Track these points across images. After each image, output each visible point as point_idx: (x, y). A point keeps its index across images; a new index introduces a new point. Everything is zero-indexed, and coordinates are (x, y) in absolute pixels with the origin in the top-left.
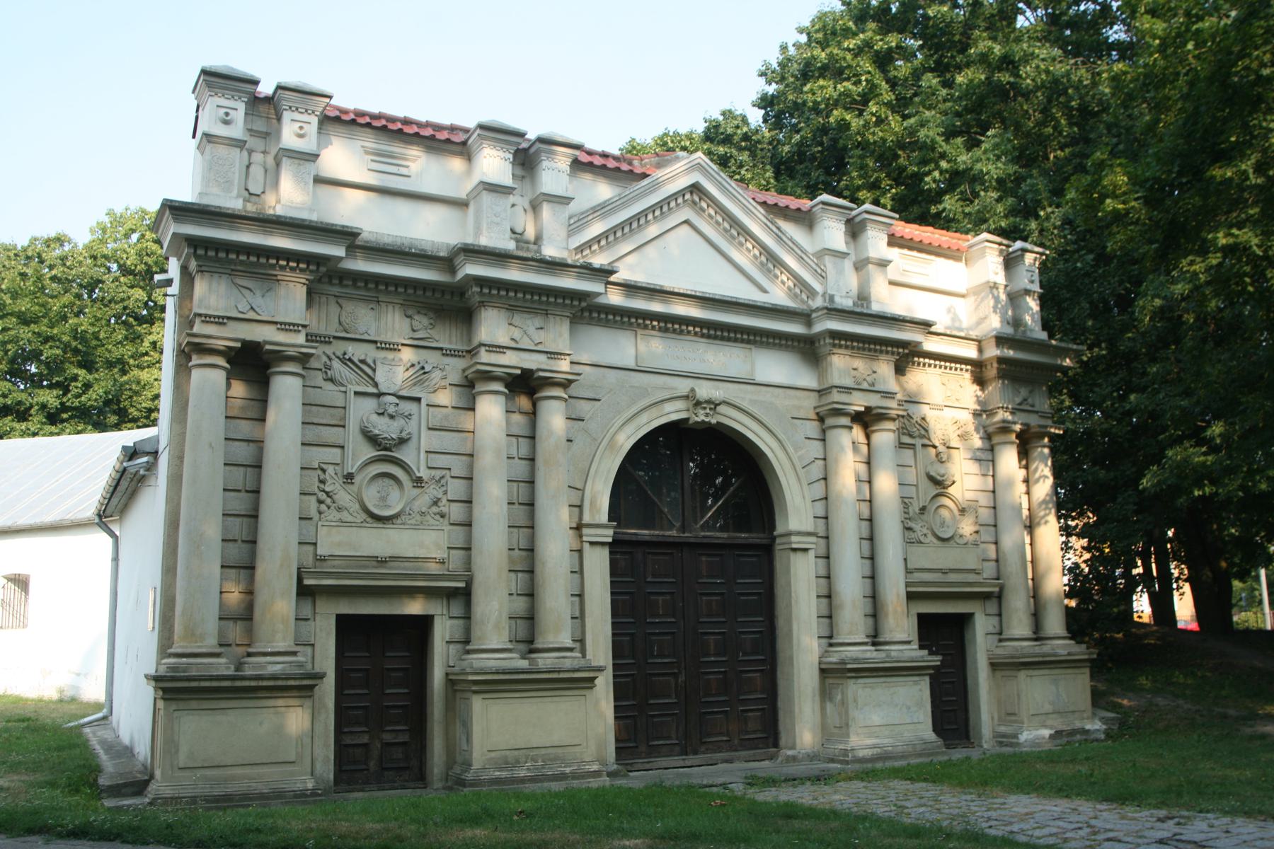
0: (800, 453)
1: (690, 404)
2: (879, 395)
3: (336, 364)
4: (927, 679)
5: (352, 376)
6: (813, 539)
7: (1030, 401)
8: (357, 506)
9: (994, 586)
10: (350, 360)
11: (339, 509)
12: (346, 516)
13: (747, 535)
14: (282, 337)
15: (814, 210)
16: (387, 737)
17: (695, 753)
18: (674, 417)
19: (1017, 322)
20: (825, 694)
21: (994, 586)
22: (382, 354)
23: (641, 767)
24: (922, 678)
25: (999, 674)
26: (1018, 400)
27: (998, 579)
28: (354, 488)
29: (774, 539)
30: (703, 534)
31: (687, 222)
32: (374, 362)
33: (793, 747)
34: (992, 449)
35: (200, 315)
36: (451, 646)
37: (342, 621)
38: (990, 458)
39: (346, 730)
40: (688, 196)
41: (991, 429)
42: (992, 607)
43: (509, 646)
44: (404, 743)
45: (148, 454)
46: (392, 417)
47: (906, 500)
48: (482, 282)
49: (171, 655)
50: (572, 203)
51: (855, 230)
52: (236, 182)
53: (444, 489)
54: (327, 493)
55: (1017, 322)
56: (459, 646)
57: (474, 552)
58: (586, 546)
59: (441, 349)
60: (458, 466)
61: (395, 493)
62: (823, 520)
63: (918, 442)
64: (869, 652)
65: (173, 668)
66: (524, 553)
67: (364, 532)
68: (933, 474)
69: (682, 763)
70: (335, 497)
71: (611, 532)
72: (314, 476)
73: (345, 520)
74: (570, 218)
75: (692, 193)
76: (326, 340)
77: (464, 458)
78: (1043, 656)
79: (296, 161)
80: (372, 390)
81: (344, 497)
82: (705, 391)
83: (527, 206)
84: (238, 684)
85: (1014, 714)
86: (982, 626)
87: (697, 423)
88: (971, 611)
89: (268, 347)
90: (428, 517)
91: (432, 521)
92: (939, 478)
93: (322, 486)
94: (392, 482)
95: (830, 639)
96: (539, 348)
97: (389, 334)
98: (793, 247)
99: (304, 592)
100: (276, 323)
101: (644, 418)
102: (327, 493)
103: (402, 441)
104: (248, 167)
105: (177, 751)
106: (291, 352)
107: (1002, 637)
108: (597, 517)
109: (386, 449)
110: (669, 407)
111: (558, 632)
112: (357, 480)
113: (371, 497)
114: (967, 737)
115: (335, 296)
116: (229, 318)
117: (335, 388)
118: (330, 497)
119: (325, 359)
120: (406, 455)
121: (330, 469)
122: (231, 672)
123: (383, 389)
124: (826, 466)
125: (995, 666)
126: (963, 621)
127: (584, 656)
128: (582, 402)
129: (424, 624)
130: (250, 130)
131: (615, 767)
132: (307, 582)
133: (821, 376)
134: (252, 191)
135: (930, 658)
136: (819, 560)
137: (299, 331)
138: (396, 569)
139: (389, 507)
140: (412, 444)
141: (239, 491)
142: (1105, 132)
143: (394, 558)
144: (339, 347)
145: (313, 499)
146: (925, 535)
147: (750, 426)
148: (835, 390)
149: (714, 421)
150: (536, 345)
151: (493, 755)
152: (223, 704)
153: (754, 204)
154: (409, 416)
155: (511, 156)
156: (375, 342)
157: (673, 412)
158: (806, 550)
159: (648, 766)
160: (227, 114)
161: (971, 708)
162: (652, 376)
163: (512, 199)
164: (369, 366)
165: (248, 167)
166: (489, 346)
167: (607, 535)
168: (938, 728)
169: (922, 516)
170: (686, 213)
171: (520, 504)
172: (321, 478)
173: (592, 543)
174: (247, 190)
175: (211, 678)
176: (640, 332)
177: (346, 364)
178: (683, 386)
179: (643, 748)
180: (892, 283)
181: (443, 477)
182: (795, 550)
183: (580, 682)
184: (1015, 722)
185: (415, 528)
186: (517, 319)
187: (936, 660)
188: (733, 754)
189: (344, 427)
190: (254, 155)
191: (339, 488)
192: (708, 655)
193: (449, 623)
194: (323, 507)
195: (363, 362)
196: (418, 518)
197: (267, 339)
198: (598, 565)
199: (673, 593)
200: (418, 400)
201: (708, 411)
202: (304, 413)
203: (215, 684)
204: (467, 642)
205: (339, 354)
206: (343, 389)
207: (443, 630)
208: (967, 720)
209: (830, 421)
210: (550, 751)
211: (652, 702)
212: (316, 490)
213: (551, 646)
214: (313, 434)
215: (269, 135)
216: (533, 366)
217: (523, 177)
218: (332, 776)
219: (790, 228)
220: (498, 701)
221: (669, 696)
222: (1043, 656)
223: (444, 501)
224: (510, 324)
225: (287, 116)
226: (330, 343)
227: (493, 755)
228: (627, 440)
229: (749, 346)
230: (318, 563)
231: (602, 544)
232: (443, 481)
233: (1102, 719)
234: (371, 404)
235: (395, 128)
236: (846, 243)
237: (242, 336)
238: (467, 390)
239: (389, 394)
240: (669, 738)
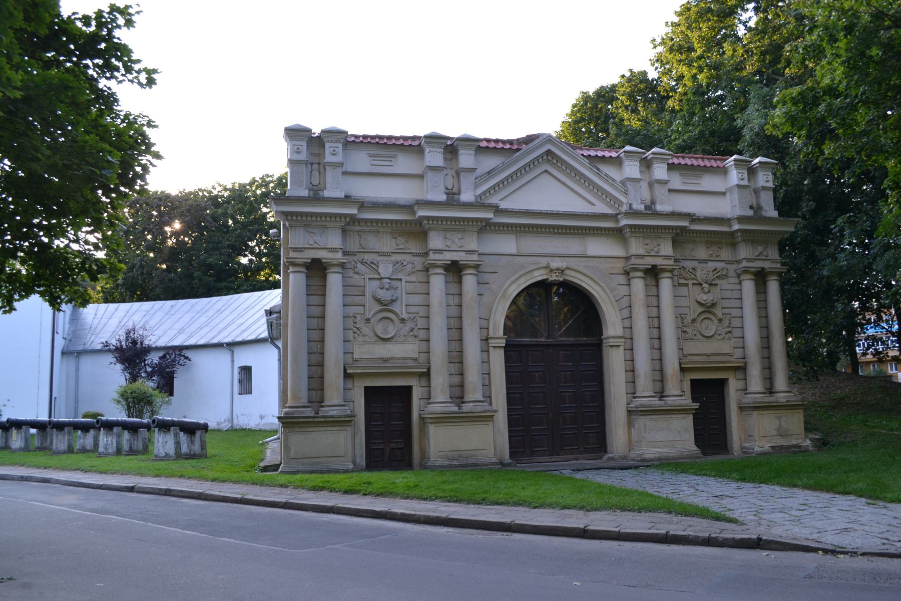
2: (662, 258)
3: (359, 265)
4: (691, 416)
5: (367, 270)
6: (623, 340)
7: (765, 253)
8: (373, 334)
9: (741, 363)
10: (366, 262)
11: (364, 336)
12: (367, 339)
13: (587, 339)
14: (330, 255)
15: (621, 155)
16: (393, 445)
17: (558, 455)
18: (539, 279)
19: (757, 209)
20: (630, 424)
21: (741, 363)
22: (382, 258)
23: (525, 461)
24: (688, 415)
25: (744, 413)
26: (756, 254)
27: (744, 359)
28: (371, 325)
29: (602, 340)
30: (560, 339)
31: (546, 171)
32: (378, 263)
33: (612, 453)
34: (740, 283)
35: (292, 248)
36: (422, 401)
37: (367, 389)
38: (739, 288)
39: (372, 442)
40: (545, 157)
41: (739, 272)
42: (740, 375)
43: (449, 400)
44: (401, 448)
45: (277, 312)
46: (387, 289)
47: (682, 316)
48: (428, 218)
49: (286, 407)
50: (477, 171)
51: (646, 164)
52: (305, 181)
54: (357, 328)
55: (757, 209)
56: (426, 401)
57: (431, 354)
59: (412, 253)
60: (422, 311)
62: (657, 329)
63: (690, 282)
64: (656, 402)
65: (285, 413)
66: (458, 353)
68: (699, 300)
69: (549, 460)
71: (504, 341)
72: (350, 322)
74: (476, 179)
75: (547, 155)
76: (353, 254)
77: (425, 307)
78: (769, 403)
79: (333, 167)
80: (379, 277)
81: (366, 330)
82: (556, 264)
83: (454, 174)
84: (316, 420)
85: (752, 436)
86: (733, 386)
87: (552, 281)
90: (408, 338)
91: (410, 340)
92: (703, 302)
93: (355, 325)
94: (390, 321)
95: (633, 394)
96: (461, 249)
97: (385, 248)
98: (607, 178)
99: (347, 376)
100: (327, 248)
101: (522, 280)
102: (357, 328)
103: (393, 301)
104: (311, 172)
105: (290, 451)
106: (335, 262)
107: (747, 392)
108: (497, 333)
109: (385, 305)
110: (536, 273)
111: (474, 393)
112: (372, 321)
113: (379, 329)
114: (726, 448)
116: (305, 248)
117: (359, 277)
119: (353, 263)
120: (396, 307)
121: (359, 317)
122: (313, 414)
124: (630, 299)
125: (741, 409)
126: (723, 383)
127: (491, 404)
128: (487, 274)
130: (311, 153)
131: (510, 461)
132: (349, 371)
133: (627, 248)
134: (314, 184)
135: (692, 404)
136: (627, 351)
138: (393, 363)
139: (388, 333)
140: (399, 302)
141: (316, 329)
142: (122, 117)
143: (391, 358)
144: (360, 257)
146: (695, 335)
147: (584, 280)
148: (633, 257)
149: (562, 279)
150: (459, 247)
151: (441, 454)
152: (311, 429)
153: (582, 157)
154: (396, 288)
155: (442, 150)
156: (378, 252)
157: (539, 276)
158: (619, 346)
159: (529, 461)
161: (728, 432)
162: (527, 258)
163: (445, 172)
164: (375, 264)
165: (311, 172)
166: (434, 250)
167: (503, 343)
168: (699, 440)
169: (693, 325)
170: (546, 167)
173: (494, 347)
175: (304, 417)
176: (518, 234)
178: (544, 261)
180: (670, 191)
181: (415, 317)
182: (612, 346)
183: (487, 418)
184: (753, 440)
185: (402, 343)
186: (449, 235)
187: (696, 405)
188: (579, 455)
189: (364, 295)
190: (314, 165)
192: (566, 404)
193: (420, 389)
194: (356, 335)
195: (372, 263)
196: (403, 338)
198: (498, 360)
199: (544, 371)
201: (557, 274)
202: (344, 290)
203: (306, 420)
204: (429, 398)
206: (363, 277)
207: (417, 394)
208: (726, 439)
209: (632, 274)
210: (470, 452)
211: (533, 428)
212: (352, 327)
213: (471, 400)
214: (349, 300)
215: (321, 154)
217: (452, 159)
218: (364, 464)
219: (606, 169)
220: (448, 427)
222: (769, 403)
223: (416, 329)
225: (327, 145)
226: (356, 255)
227: (441, 454)
228: (514, 291)
229: (582, 237)
230: (354, 362)
232: (415, 320)
233: (810, 439)
234: (376, 283)
235: (400, 143)
236: (641, 172)
238: (425, 273)
240: (543, 447)
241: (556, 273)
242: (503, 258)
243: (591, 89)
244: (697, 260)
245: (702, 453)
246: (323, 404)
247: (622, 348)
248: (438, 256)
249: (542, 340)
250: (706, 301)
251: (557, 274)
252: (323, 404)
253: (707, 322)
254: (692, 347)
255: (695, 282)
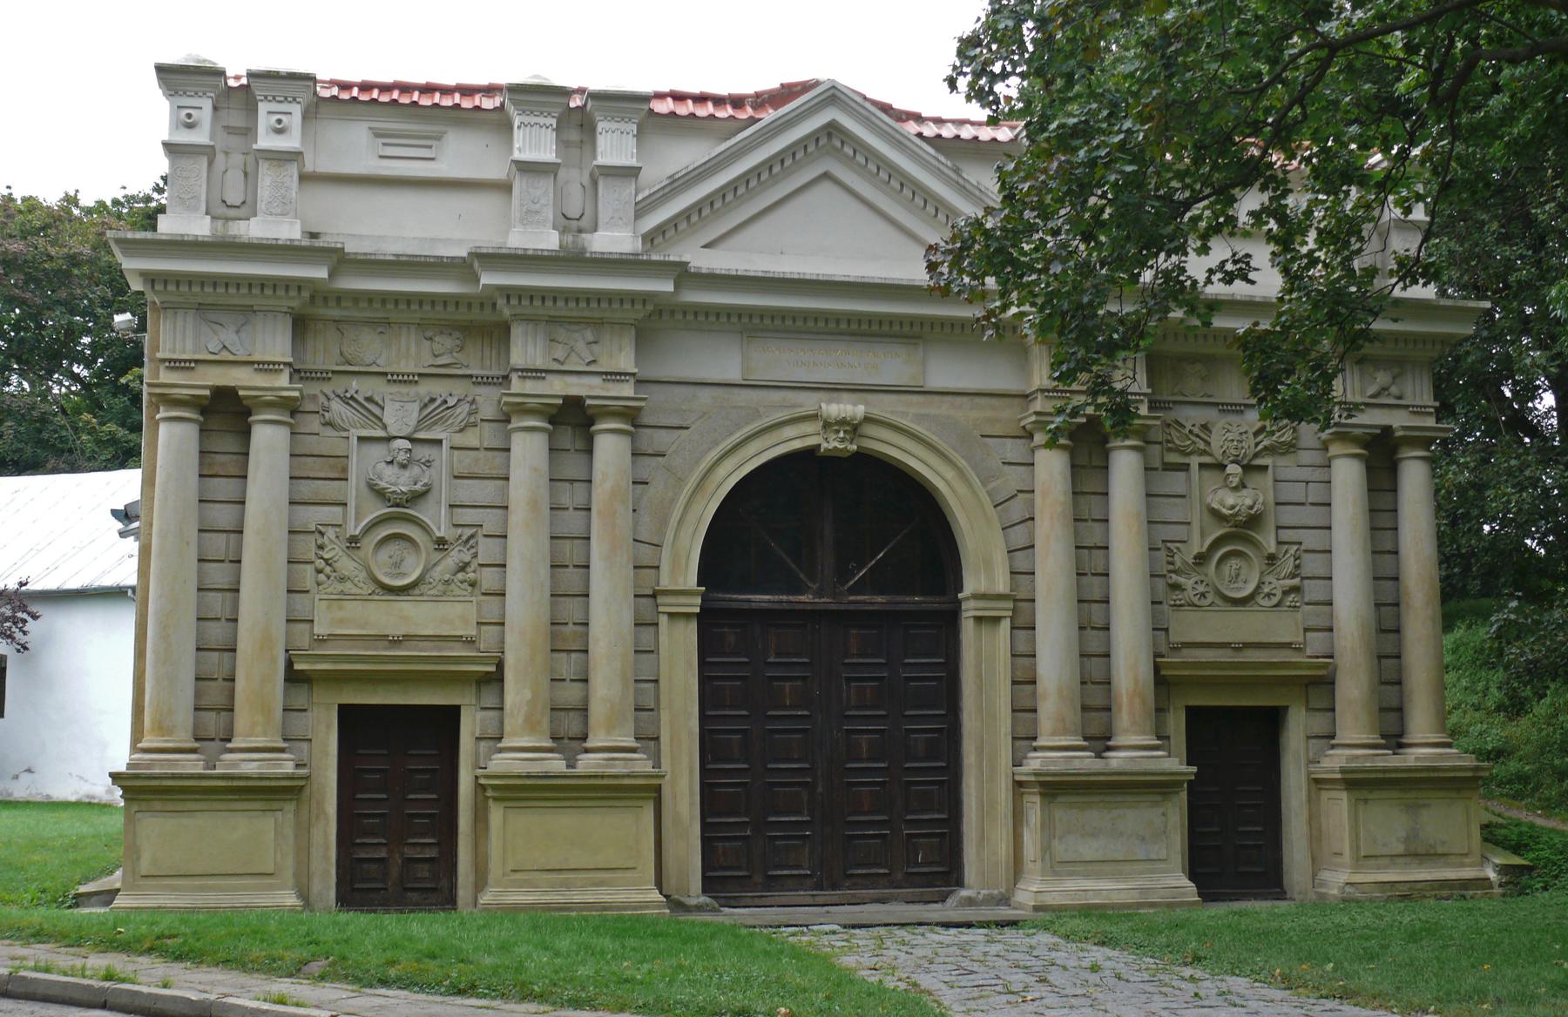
0: (991, 486)
1: (860, 431)
5: (357, 417)
7: (1394, 390)
10: (352, 398)
11: (342, 580)
13: (921, 599)
14: (261, 380)
16: (411, 853)
17: (834, 887)
18: (797, 445)
23: (750, 902)
29: (959, 602)
30: (852, 598)
31: (826, 176)
36: (483, 744)
37: (346, 712)
53: (473, 551)
54: (326, 561)
57: (1403, 606)
58: (663, 620)
59: (471, 376)
61: (410, 559)
67: (372, 605)
68: (1215, 506)
69: (810, 901)
70: (335, 565)
71: (698, 600)
73: (349, 592)
76: (324, 376)
80: (380, 433)
87: (827, 450)
88: (1285, 704)
89: (589, 402)
90: (453, 586)
91: (457, 592)
92: (1224, 511)
94: (408, 544)
95: (1025, 739)
100: (253, 363)
102: (326, 561)
103: (416, 497)
105: (138, 858)
108: (681, 580)
109: (397, 505)
115: (335, 321)
117: (336, 434)
118: (330, 565)
119: (322, 399)
121: (331, 533)
123: (393, 431)
129: (453, 713)
132: (297, 667)
137: (282, 370)
139: (404, 575)
141: (222, 561)
144: (339, 384)
145: (309, 569)
150: (589, 364)
156: (385, 374)
157: (793, 440)
159: (757, 902)
160: (279, 121)
171: (575, 566)
172: (319, 542)
173: (671, 615)
174: (224, 202)
177: (348, 404)
179: (758, 878)
181: (472, 536)
191: (341, 553)
193: (480, 715)
194: (322, 577)
196: (441, 587)
197: (239, 384)
200: (439, 442)
205: (340, 391)
206: (344, 434)
214: (306, 489)
216: (582, 392)
221: (799, 813)
224: (552, 340)
225: (263, 108)
231: (687, 616)
234: (377, 452)
237: (210, 383)
239: (401, 438)
240: (798, 867)
241: (838, 432)
242: (705, 395)
243: (955, 53)
244: (1217, 404)
245: (1200, 895)
246: (1111, 743)
247: (1006, 625)
248: (530, 387)
249: (802, 598)
250: (1233, 507)
251: (841, 435)
252: (1034, 744)
253: (1234, 563)
254: (1194, 627)
255: (1207, 459)
